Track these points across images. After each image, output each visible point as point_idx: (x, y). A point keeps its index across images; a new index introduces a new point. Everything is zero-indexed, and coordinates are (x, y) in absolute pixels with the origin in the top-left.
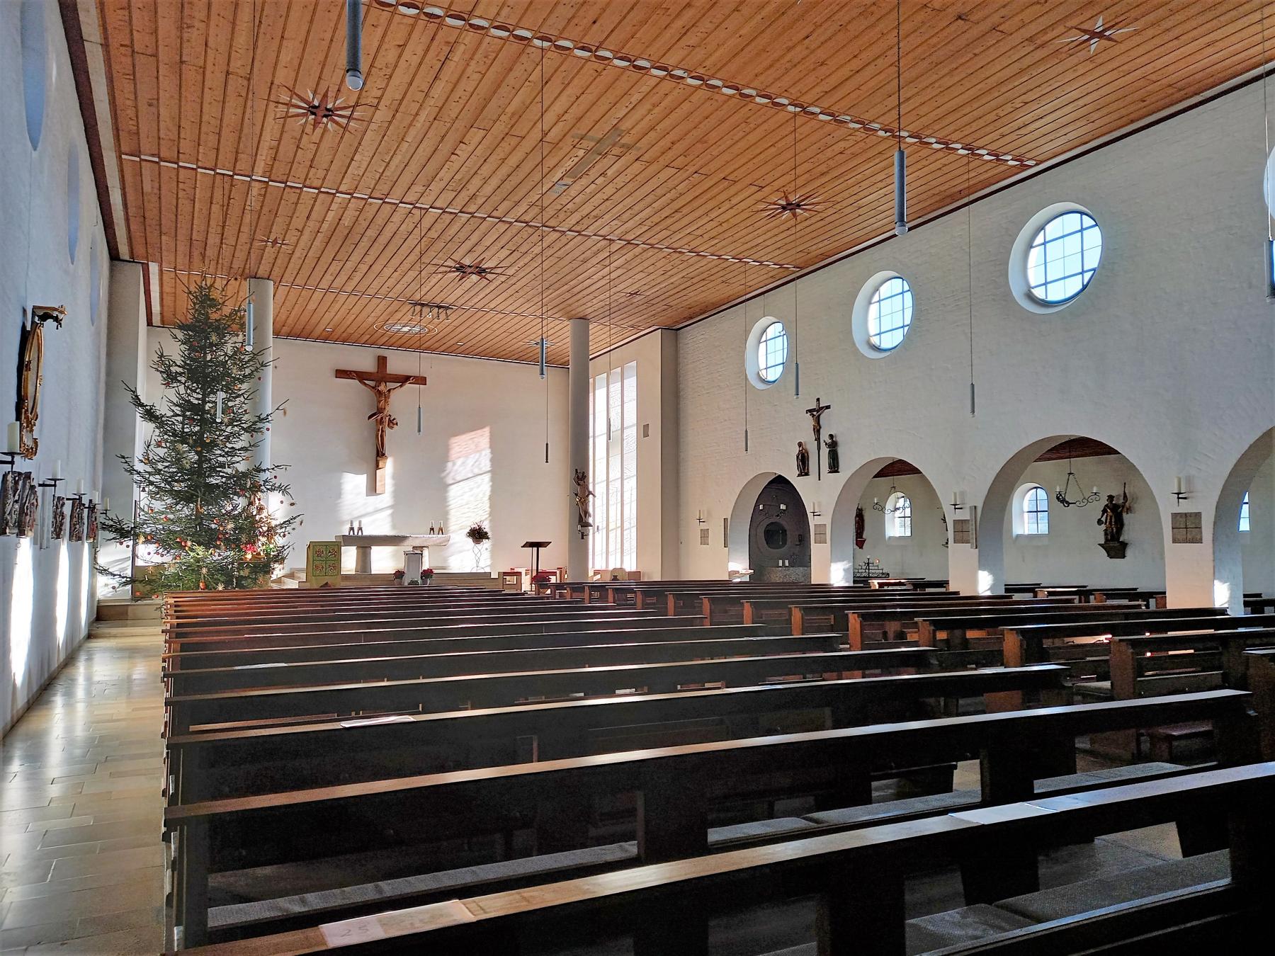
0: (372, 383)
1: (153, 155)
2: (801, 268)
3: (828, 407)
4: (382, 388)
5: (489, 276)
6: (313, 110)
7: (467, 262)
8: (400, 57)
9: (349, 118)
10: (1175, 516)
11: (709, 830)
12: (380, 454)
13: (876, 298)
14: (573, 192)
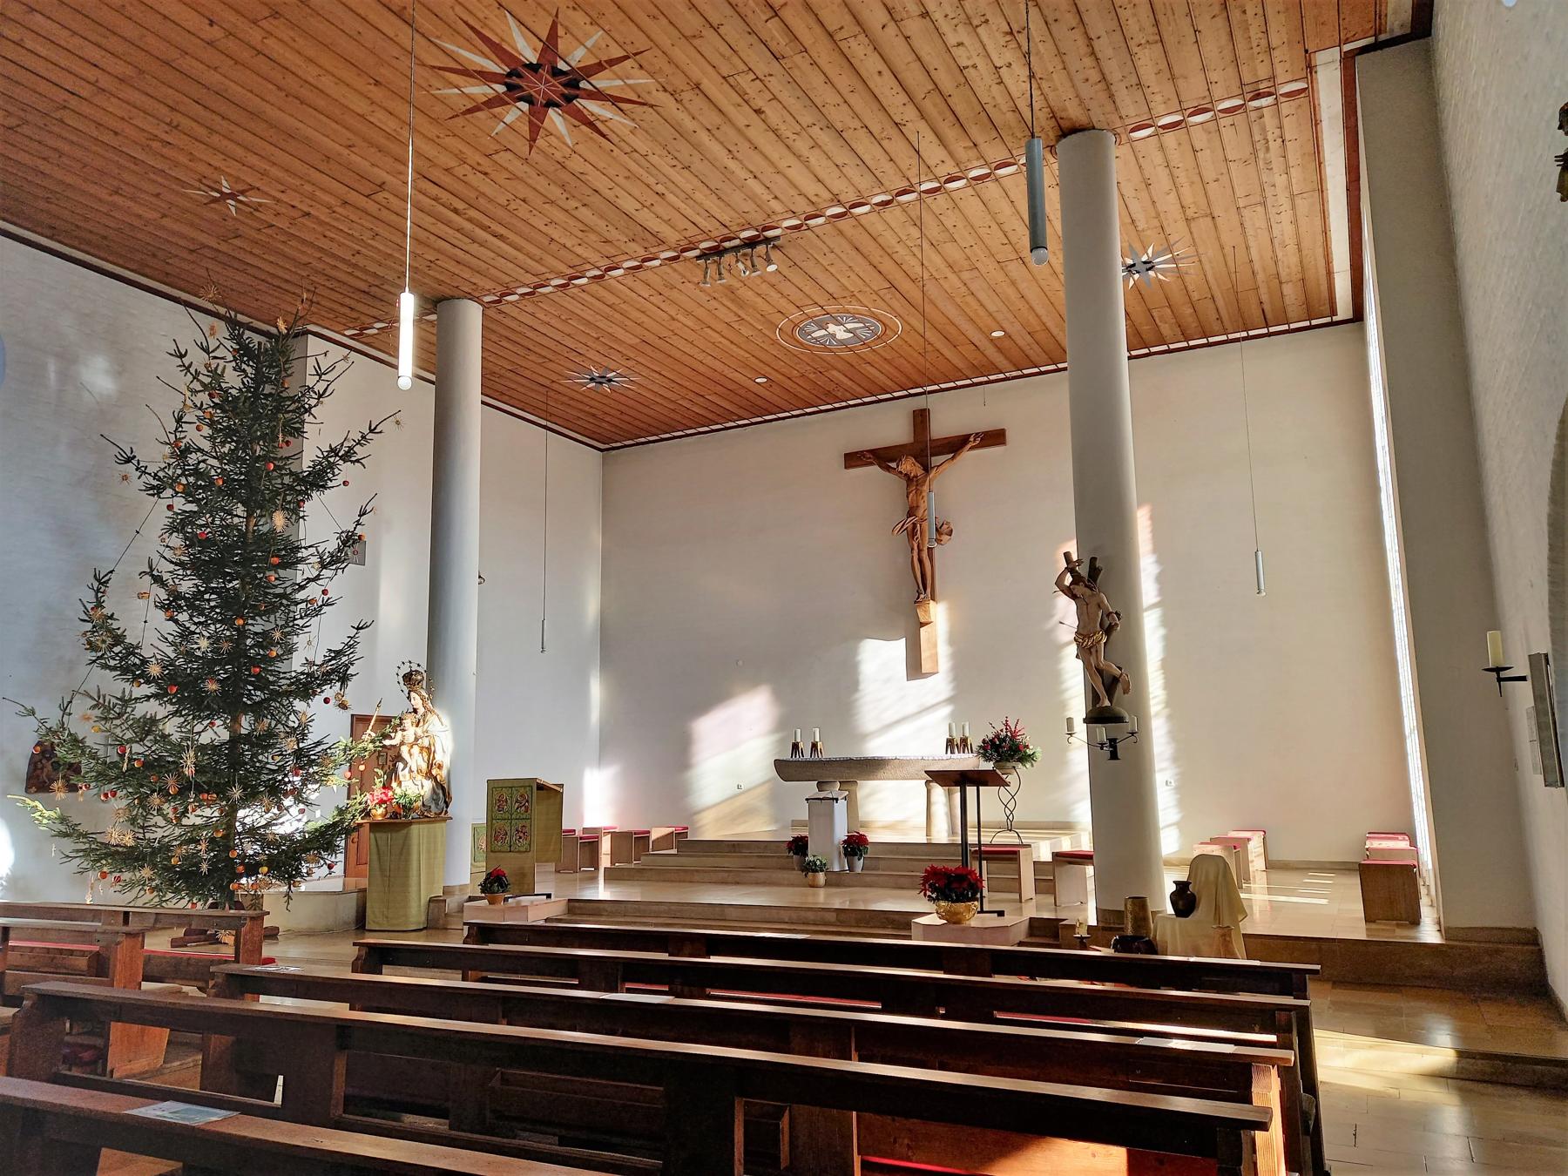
0: (893, 465)
11: (566, 825)
12: (923, 586)
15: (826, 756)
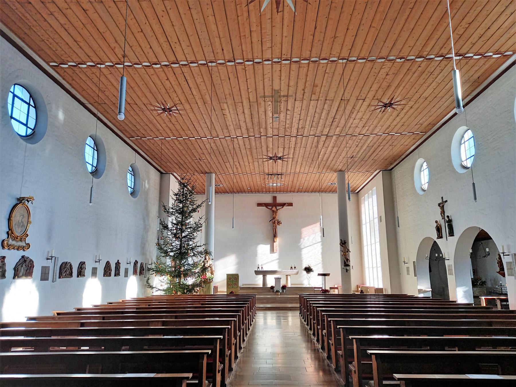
0: (270, 207)
2: (426, 132)
4: (274, 209)
12: (275, 236)
13: (463, 142)
15: (264, 270)
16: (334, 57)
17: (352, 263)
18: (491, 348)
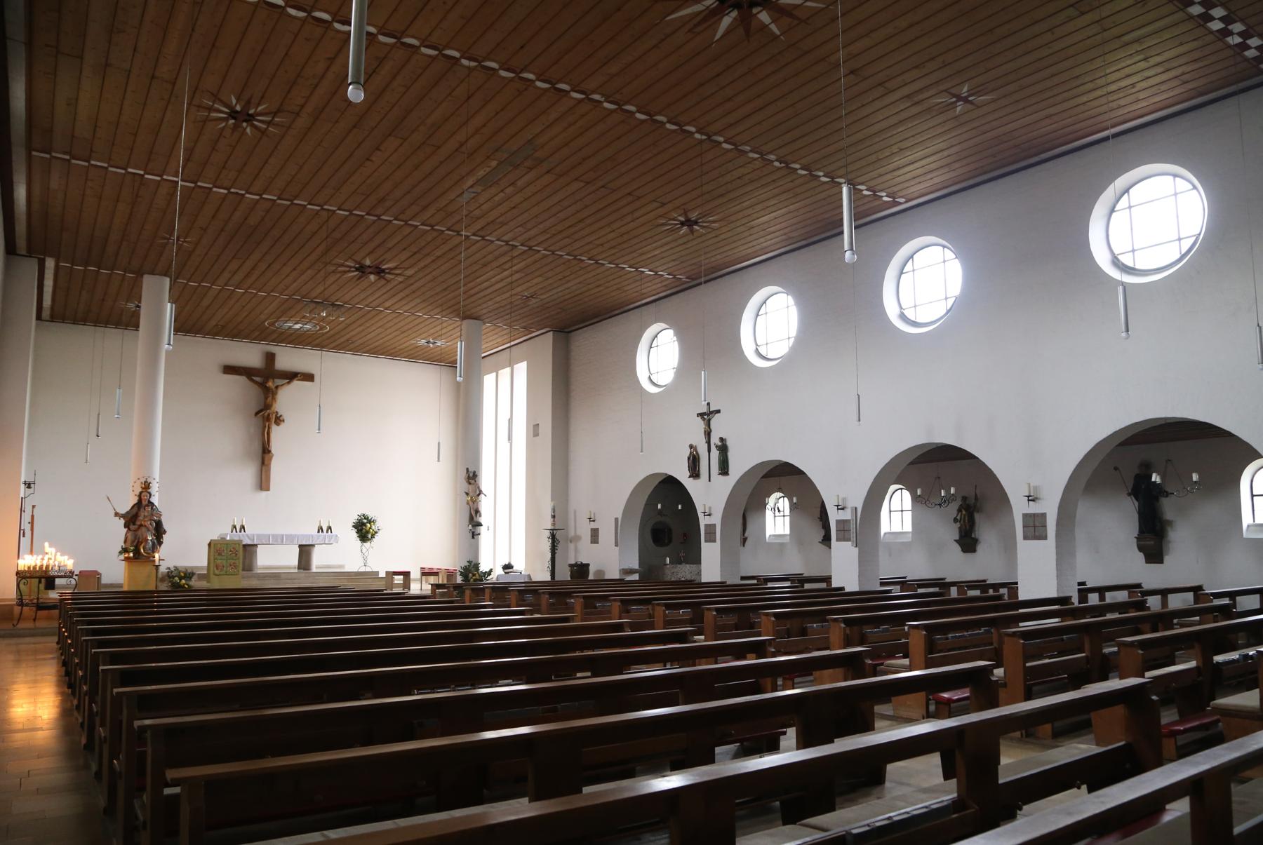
0: (258, 379)
1: (65, 153)
3: (718, 411)
4: (270, 384)
5: (388, 276)
6: (233, 114)
7: (368, 262)
8: (328, 68)
9: (269, 123)
10: (1025, 516)
14: (482, 200)
16: (325, 11)
17: (485, 519)
18: (660, 666)
